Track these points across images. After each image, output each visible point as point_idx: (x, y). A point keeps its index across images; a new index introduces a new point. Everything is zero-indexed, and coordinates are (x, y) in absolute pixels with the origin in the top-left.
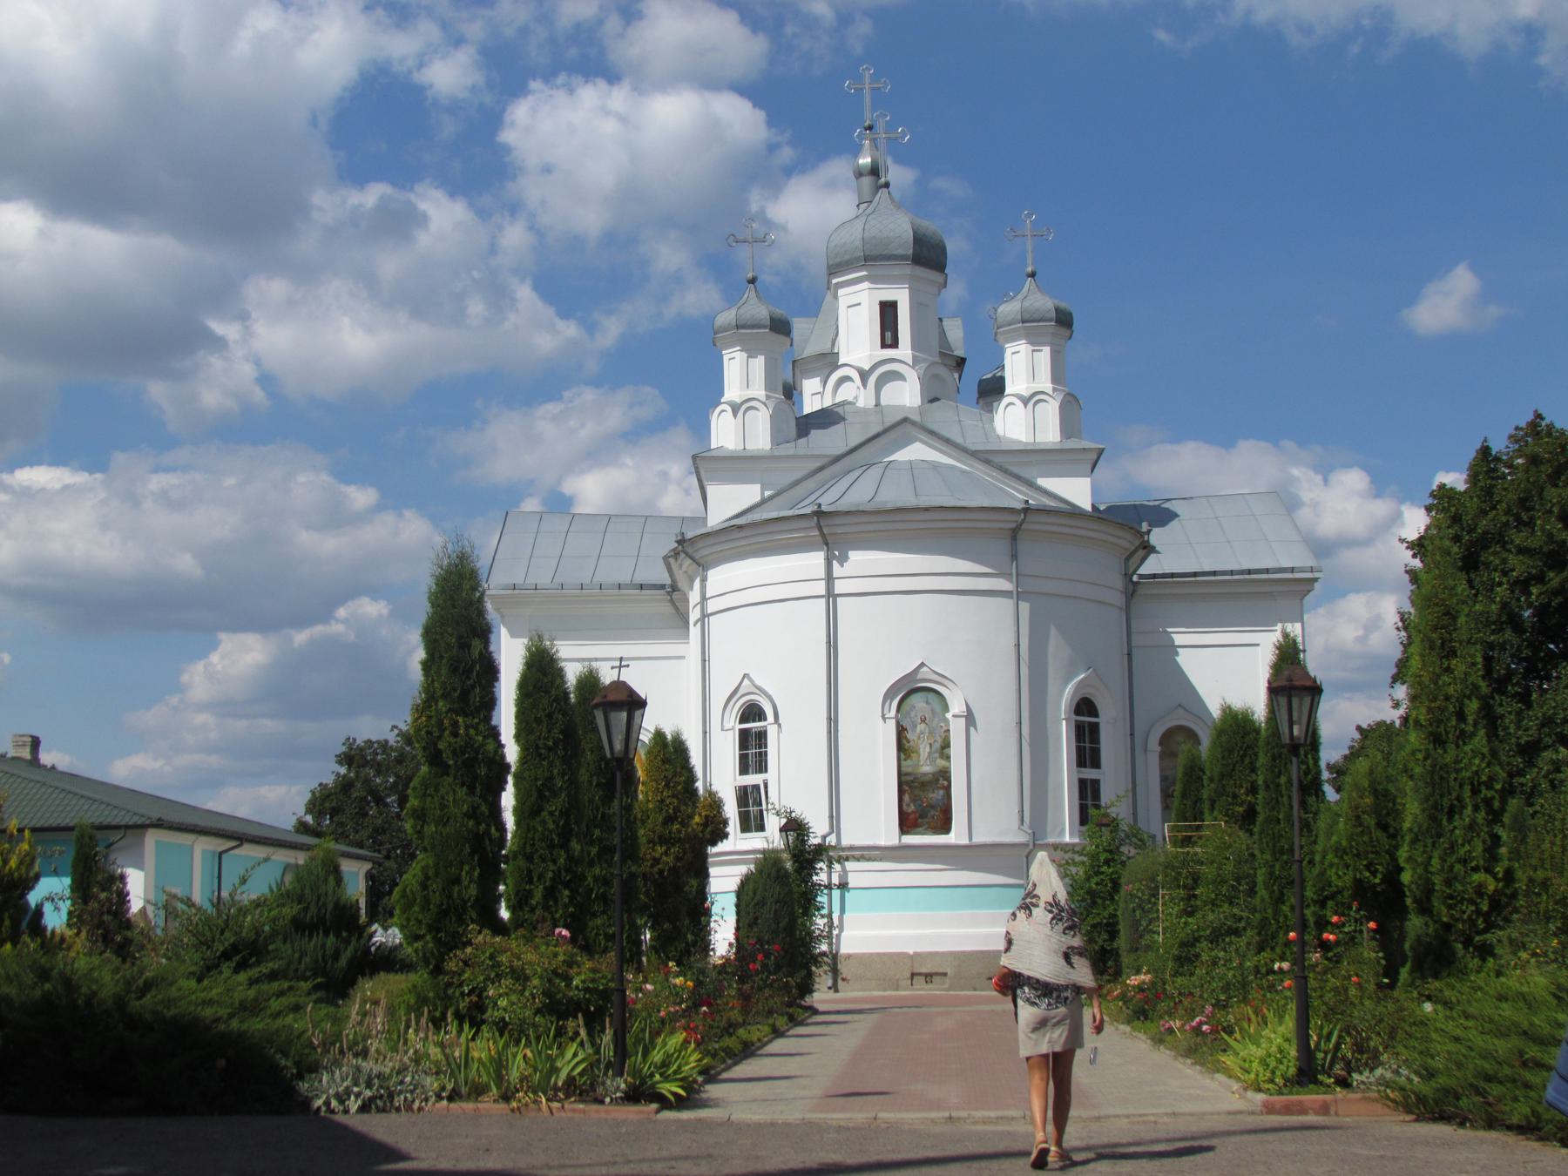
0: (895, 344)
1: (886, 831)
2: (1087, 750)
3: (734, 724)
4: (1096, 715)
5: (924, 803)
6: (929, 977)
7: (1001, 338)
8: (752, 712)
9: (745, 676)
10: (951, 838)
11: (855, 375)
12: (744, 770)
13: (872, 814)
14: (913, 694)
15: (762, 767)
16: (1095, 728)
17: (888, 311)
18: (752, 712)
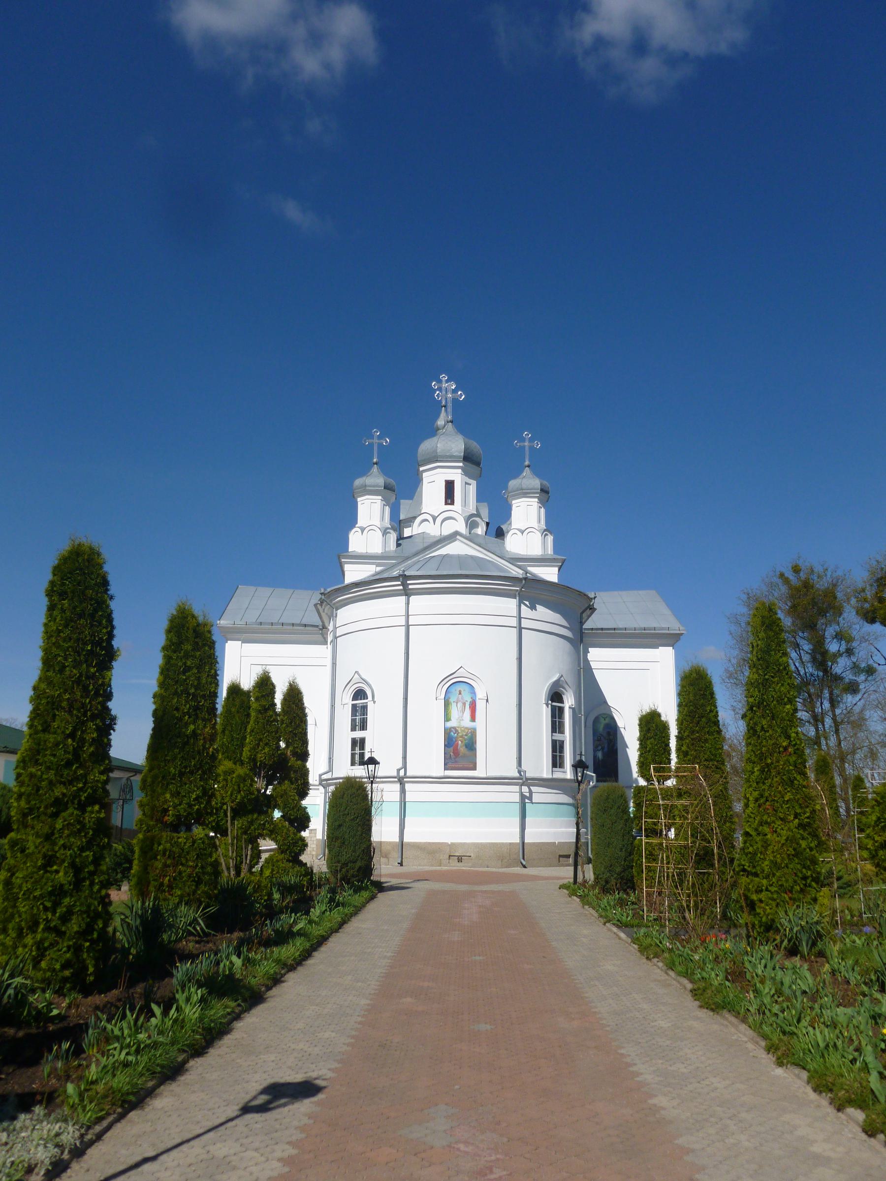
0: (452, 503)
1: (437, 767)
2: (557, 726)
3: (349, 702)
5: (460, 751)
6: (460, 859)
7: (510, 499)
8: (360, 694)
10: (479, 772)
11: (431, 519)
12: (353, 729)
13: (429, 756)
14: (457, 689)
15: (363, 727)
17: (450, 486)
18: (360, 694)
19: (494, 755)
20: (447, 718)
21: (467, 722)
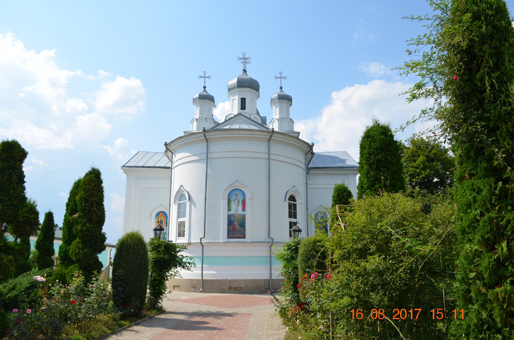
2: (292, 212)
4: (296, 202)
9: (181, 186)
16: (295, 205)
19: (254, 229)
20: (229, 209)
21: (240, 212)
